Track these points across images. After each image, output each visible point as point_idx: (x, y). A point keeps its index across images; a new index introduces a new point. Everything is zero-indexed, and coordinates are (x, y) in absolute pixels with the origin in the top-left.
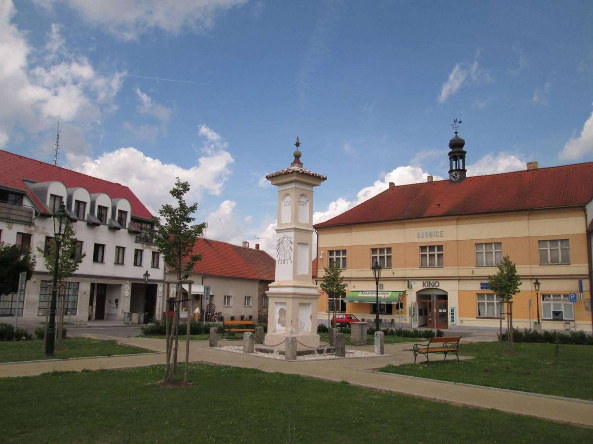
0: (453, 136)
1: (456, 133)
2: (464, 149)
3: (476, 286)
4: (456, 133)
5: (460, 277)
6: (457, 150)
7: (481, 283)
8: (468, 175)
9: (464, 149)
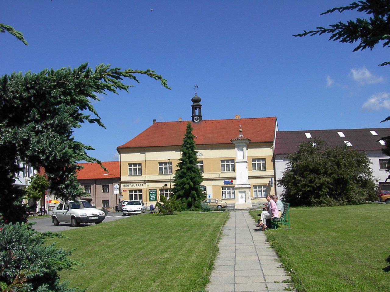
0: (193, 96)
1: (196, 93)
2: (200, 103)
3: (222, 183)
4: (196, 93)
5: (213, 178)
6: (196, 104)
7: (225, 181)
8: (203, 119)
9: (200, 103)
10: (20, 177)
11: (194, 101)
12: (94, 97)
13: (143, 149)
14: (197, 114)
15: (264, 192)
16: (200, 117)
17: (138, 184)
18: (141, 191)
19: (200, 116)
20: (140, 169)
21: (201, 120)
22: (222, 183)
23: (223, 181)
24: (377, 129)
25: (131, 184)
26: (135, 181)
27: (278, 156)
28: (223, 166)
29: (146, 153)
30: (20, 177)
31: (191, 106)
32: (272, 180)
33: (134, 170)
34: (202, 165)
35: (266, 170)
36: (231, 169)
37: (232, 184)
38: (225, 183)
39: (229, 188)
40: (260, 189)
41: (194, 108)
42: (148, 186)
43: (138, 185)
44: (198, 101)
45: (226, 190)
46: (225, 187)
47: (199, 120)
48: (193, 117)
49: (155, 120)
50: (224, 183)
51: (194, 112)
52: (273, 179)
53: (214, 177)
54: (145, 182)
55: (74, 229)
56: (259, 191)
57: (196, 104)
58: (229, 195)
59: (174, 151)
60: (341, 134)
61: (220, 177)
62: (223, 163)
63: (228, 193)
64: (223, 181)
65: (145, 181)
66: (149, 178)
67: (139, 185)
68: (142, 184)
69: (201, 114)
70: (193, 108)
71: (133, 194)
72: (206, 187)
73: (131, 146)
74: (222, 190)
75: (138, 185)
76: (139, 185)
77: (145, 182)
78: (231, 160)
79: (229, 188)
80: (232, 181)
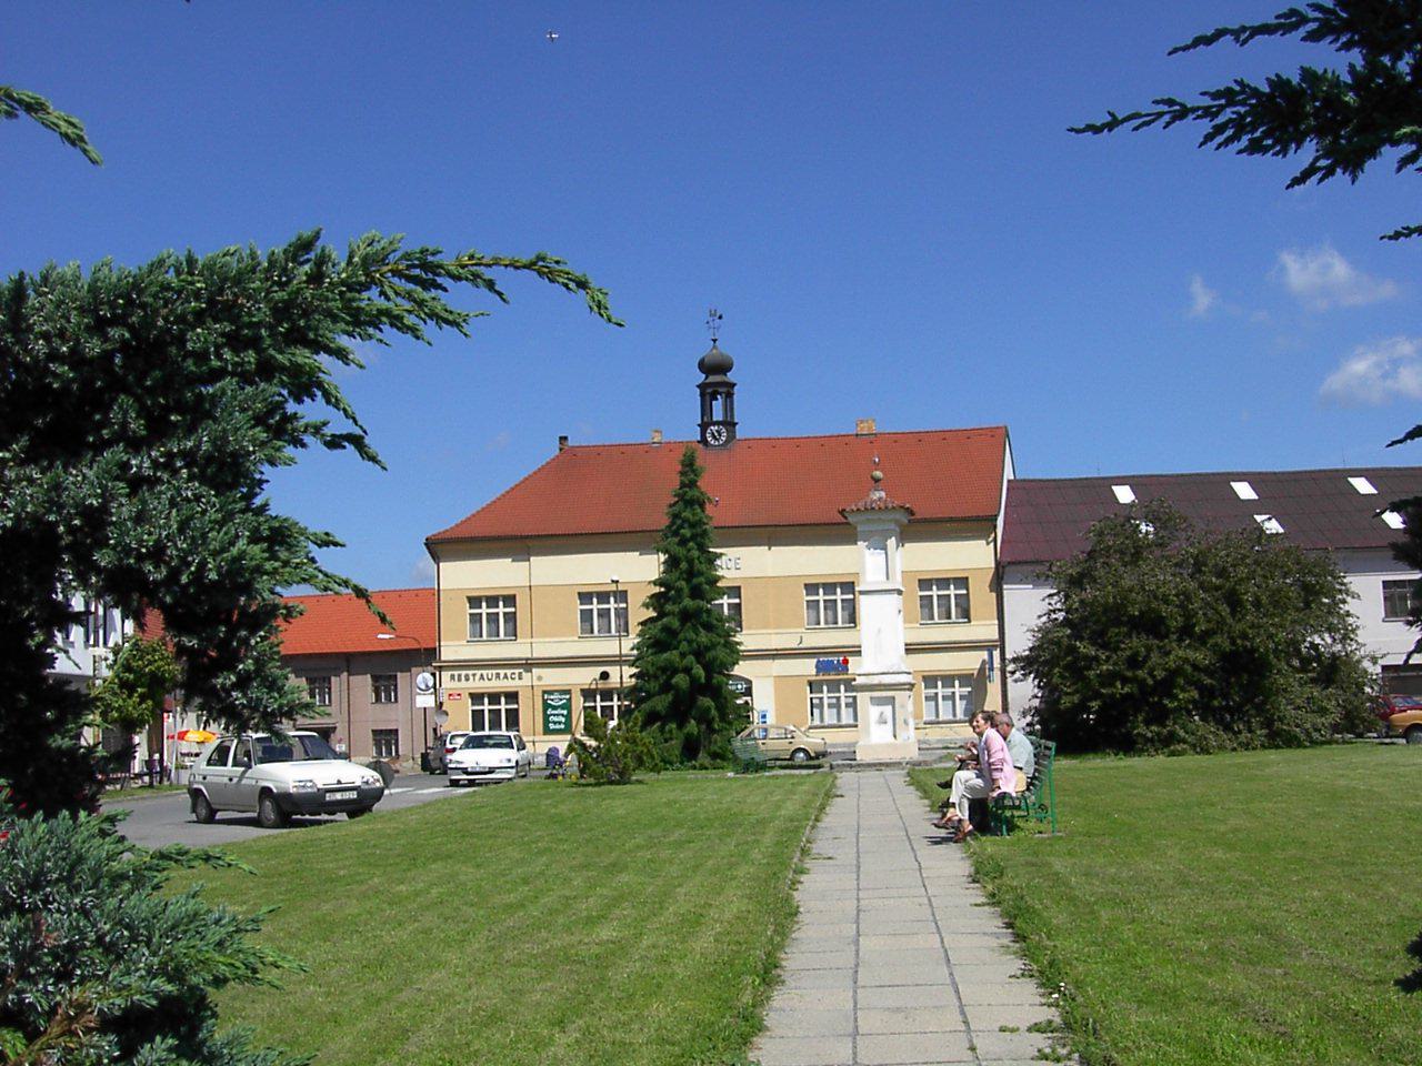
0: (704, 350)
1: (715, 341)
2: (731, 377)
3: (808, 667)
4: (715, 341)
5: (776, 650)
6: (716, 380)
7: (819, 661)
8: (740, 433)
9: (731, 377)
10: (73, 647)
11: (706, 367)
12: (341, 354)
13: (520, 545)
14: (718, 415)
15: (964, 702)
16: (730, 428)
17: (502, 672)
18: (512, 697)
19: (730, 424)
20: (511, 618)
21: (731, 436)
22: (808, 667)
23: (814, 661)
24: (1373, 470)
25: (479, 672)
26: (492, 660)
27: (1013, 568)
28: (813, 605)
29: (532, 559)
30: (73, 647)
31: (698, 386)
32: (991, 656)
33: (488, 621)
34: (737, 601)
35: (969, 621)
36: (842, 615)
37: (846, 670)
38: (820, 668)
39: (834, 686)
40: (948, 691)
41: (708, 393)
42: (540, 678)
43: (502, 676)
44: (722, 367)
45: (825, 695)
46: (821, 683)
47: (724, 439)
48: (704, 427)
49: (566, 438)
50: (817, 666)
51: (706, 410)
52: (996, 654)
53: (779, 647)
54: (528, 665)
55: (269, 836)
56: (944, 698)
57: (716, 380)
58: (835, 710)
59: (634, 551)
60: (1244, 491)
61: (801, 646)
62: (811, 595)
63: (830, 706)
64: (814, 661)
65: (527, 659)
66: (544, 649)
67: (506, 676)
68: (517, 671)
69: (732, 416)
70: (703, 395)
71: (486, 707)
72: (751, 682)
73: (477, 532)
74: (811, 692)
75: (502, 676)
76: (506, 676)
77: (528, 665)
78: (843, 585)
79: (834, 686)
80: (846, 662)
